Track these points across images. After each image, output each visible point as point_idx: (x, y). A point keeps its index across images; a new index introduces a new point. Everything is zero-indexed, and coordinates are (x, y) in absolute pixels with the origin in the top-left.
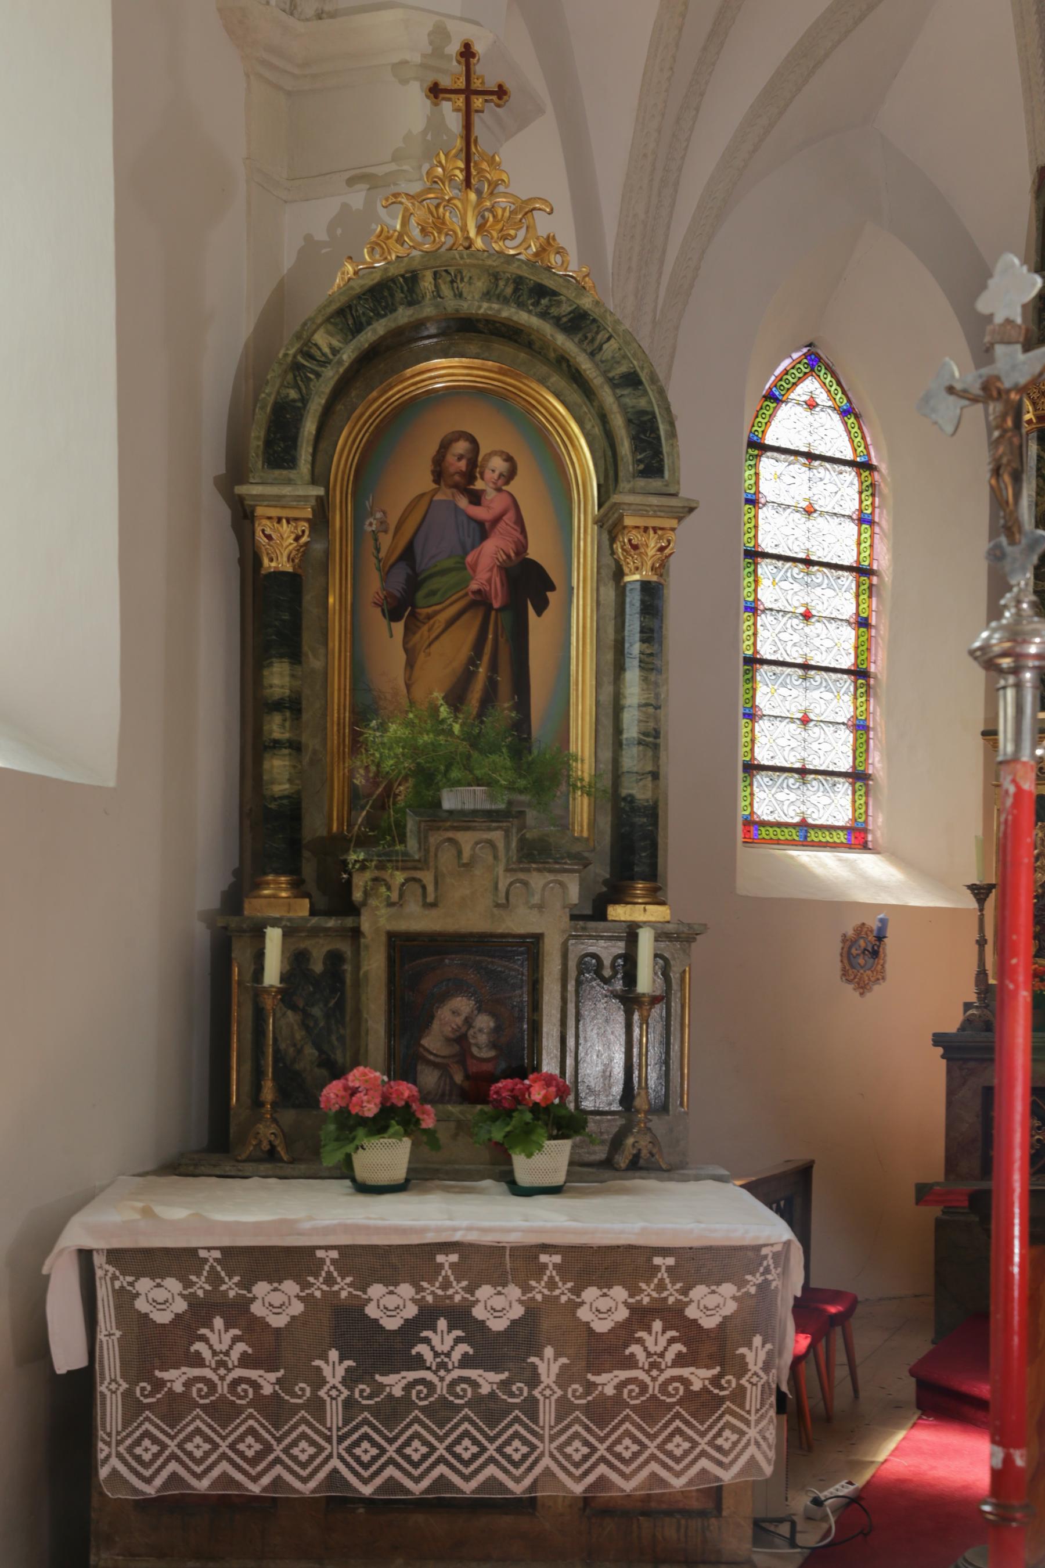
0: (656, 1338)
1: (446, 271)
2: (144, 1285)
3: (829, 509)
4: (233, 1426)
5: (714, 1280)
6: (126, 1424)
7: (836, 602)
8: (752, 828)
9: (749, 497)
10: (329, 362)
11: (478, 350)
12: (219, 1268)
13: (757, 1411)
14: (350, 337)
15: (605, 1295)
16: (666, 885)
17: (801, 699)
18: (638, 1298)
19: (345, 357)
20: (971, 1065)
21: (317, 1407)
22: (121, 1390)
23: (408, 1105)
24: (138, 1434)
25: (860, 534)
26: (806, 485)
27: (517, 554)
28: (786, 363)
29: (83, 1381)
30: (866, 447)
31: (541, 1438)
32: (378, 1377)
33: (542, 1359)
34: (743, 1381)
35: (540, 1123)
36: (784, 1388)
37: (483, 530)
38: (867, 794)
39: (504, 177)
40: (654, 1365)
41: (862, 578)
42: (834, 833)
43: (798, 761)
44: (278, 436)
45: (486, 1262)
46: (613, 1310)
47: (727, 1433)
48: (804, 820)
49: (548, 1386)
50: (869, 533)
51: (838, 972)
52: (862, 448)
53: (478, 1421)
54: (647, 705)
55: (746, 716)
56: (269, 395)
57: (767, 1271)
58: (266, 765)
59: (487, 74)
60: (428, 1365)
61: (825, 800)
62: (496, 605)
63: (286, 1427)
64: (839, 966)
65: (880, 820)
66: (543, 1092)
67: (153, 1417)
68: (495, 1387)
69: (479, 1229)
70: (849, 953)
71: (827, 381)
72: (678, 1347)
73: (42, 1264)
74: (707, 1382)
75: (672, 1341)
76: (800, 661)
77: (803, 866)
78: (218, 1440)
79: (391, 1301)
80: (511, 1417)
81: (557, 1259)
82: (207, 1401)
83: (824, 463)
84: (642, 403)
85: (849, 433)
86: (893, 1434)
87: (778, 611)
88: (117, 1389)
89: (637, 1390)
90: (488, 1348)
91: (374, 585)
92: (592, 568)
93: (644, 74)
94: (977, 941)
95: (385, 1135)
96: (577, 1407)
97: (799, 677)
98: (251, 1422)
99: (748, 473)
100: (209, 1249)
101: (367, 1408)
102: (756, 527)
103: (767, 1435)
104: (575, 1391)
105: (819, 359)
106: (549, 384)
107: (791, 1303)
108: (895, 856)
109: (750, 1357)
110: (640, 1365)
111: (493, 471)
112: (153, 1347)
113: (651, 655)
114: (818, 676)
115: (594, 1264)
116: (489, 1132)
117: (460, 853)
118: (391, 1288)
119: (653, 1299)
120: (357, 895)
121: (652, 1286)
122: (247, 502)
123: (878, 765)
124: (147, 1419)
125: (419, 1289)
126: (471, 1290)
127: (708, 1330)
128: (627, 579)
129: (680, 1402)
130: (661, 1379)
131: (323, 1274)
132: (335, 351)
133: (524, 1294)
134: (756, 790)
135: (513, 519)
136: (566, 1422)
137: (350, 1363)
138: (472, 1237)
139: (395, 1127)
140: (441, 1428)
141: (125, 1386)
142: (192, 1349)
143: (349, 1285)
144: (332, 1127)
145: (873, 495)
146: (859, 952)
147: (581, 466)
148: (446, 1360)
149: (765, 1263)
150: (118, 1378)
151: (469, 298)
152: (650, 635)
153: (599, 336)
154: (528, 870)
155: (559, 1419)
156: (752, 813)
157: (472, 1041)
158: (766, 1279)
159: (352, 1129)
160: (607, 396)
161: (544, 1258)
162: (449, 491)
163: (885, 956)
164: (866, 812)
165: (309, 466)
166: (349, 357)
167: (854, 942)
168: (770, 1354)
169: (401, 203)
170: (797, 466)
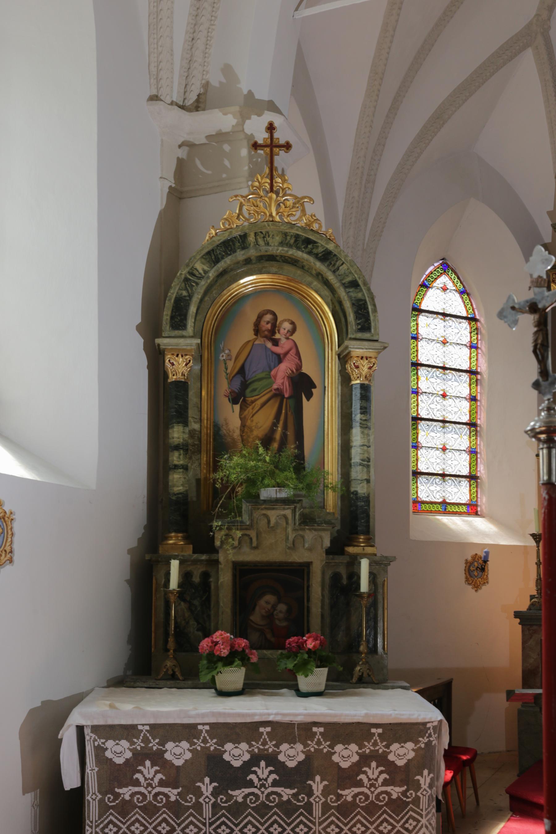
0: (373, 771)
1: (261, 232)
2: (110, 744)
3: (454, 341)
4: (155, 817)
5: (402, 740)
6: (100, 817)
7: (459, 388)
8: (417, 505)
9: (413, 336)
10: (203, 277)
11: (276, 270)
12: (148, 735)
13: (426, 809)
14: (213, 265)
15: (346, 748)
16: (374, 536)
17: (441, 438)
18: (363, 750)
19: (210, 275)
20: (535, 627)
21: (198, 807)
22: (98, 798)
23: (243, 650)
24: (106, 822)
25: (471, 354)
26: (443, 329)
27: (297, 370)
28: (431, 268)
29: (79, 793)
30: (473, 310)
31: (314, 824)
32: (230, 792)
33: (314, 782)
34: (419, 794)
35: (312, 659)
36: (440, 797)
37: (280, 359)
38: (477, 486)
39: (290, 187)
40: (372, 785)
41: (472, 376)
42: (460, 507)
43: (441, 470)
44: (177, 314)
45: (285, 731)
46: (351, 756)
47: (411, 821)
48: (444, 500)
49: (318, 796)
50: (475, 353)
51: (464, 579)
52: (471, 310)
53: (281, 815)
54: (363, 445)
55: (413, 447)
56: (173, 294)
57: (430, 736)
58: (171, 477)
59: (281, 136)
60: (256, 785)
61: (455, 490)
62: (286, 395)
63: (183, 818)
64: (463, 576)
65: (484, 500)
66: (314, 643)
67: (114, 813)
68: (290, 797)
69: (281, 714)
70: (469, 569)
71: (452, 277)
72: (384, 776)
73: (59, 733)
74: (400, 794)
75: (381, 772)
76: (441, 418)
77: (444, 524)
78: (147, 825)
79: (236, 752)
80: (299, 812)
81: (322, 729)
82: (142, 804)
83: (452, 318)
84: (360, 295)
85: (464, 303)
86: (498, 824)
87: (429, 393)
88: (96, 798)
89: (364, 798)
90: (286, 776)
91: (224, 387)
92: (335, 377)
93: (357, 129)
94: (536, 563)
95: (233, 666)
96: (333, 807)
97: (441, 427)
98: (164, 815)
99: (412, 324)
100: (143, 725)
101: (224, 808)
102: (417, 351)
103: (432, 822)
104: (331, 799)
105: (448, 266)
106: (312, 286)
107: (443, 752)
108: (492, 519)
109: (422, 781)
110: (365, 785)
111: (285, 329)
112: (116, 776)
113: (365, 420)
114: (450, 426)
115: (341, 732)
116: (286, 664)
117: (269, 522)
118: (236, 745)
119: (371, 751)
120: (218, 543)
121: (371, 744)
122: (161, 347)
123: (483, 472)
124: (111, 814)
125: (251, 746)
126: (277, 746)
127: (400, 767)
128: (353, 382)
129: (386, 805)
130: (376, 792)
131: (202, 738)
132: (206, 272)
133: (305, 748)
134: (419, 485)
135: (295, 353)
136: (327, 815)
137: (215, 784)
138: (278, 718)
139: (237, 662)
140: (262, 818)
141: (100, 796)
142: (135, 777)
143: (215, 744)
144: (205, 662)
145: (477, 334)
146: (474, 569)
147: (330, 326)
148: (265, 782)
149: (429, 732)
150: (96, 793)
151: (272, 245)
152: (365, 410)
153: (338, 263)
154: (304, 530)
155: (323, 814)
156: (417, 497)
157: (276, 617)
158: (430, 740)
159: (215, 663)
160: (342, 293)
161: (315, 729)
162: (262, 339)
163: (488, 570)
164: (477, 496)
165: (192, 328)
166: (213, 274)
167: (471, 564)
168: (432, 779)
169: (238, 200)
170: (438, 320)
